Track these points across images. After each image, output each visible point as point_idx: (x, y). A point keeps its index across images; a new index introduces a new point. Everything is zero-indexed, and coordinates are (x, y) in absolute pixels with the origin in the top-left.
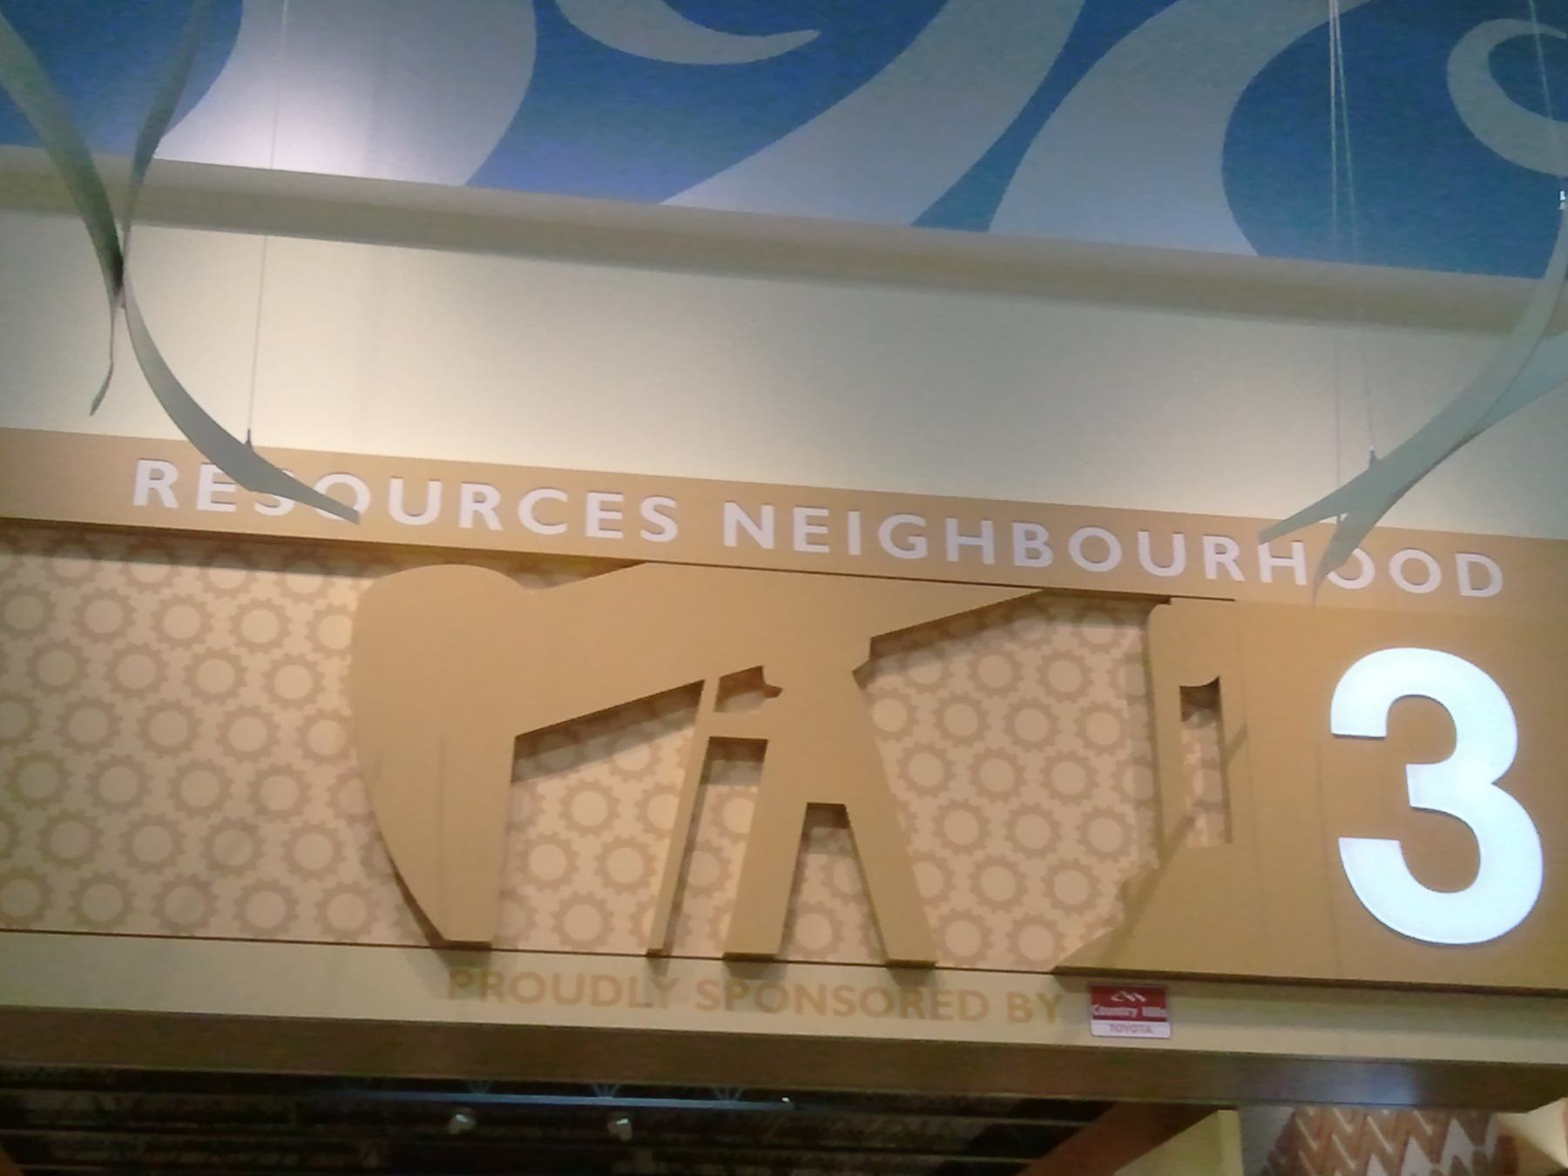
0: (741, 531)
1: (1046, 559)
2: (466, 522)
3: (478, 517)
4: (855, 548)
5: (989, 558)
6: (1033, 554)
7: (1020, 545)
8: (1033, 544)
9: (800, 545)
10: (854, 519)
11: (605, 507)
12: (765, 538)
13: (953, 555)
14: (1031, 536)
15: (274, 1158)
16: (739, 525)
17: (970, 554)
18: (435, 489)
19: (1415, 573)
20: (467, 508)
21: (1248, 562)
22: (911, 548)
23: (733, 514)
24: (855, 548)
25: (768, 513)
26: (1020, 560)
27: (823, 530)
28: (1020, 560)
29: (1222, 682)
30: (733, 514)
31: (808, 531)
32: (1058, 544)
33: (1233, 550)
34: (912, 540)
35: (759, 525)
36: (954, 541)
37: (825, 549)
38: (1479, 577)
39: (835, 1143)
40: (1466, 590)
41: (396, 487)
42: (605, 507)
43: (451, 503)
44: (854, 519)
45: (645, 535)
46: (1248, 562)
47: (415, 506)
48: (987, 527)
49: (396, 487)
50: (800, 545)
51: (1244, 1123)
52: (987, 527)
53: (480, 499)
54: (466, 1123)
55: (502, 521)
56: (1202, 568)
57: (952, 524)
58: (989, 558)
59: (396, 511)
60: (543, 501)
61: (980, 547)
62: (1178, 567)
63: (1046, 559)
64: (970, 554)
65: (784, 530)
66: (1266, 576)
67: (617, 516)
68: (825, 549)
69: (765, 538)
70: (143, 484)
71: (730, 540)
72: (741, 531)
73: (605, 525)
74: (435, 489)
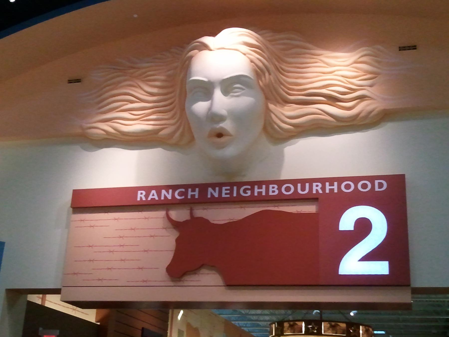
2: (314, 192)
3: (317, 190)
4: (235, 195)
5: (264, 194)
6: (273, 192)
7: (271, 189)
8: (273, 190)
9: (224, 195)
10: (235, 188)
11: (226, 190)
12: (216, 195)
16: (165, 195)
18: (307, 185)
21: (323, 188)
22: (247, 193)
23: (210, 190)
24: (235, 195)
28: (271, 194)
29: (360, 257)
30: (210, 190)
31: (262, 190)
32: (279, 189)
33: (320, 185)
34: (247, 191)
35: (165, 195)
36: (328, 187)
37: (228, 196)
38: (381, 185)
40: (377, 189)
41: (299, 185)
42: (226, 190)
44: (235, 188)
46: (323, 188)
47: (303, 189)
48: (264, 187)
49: (299, 185)
50: (224, 195)
54: (269, 103)
55: (322, 191)
56: (312, 191)
58: (264, 194)
59: (300, 191)
60: (181, 191)
61: (334, 189)
62: (307, 191)
65: (220, 192)
66: (327, 191)
67: (228, 192)
68: (228, 196)
69: (169, 197)
70: (139, 196)
73: (226, 194)
74: (307, 185)
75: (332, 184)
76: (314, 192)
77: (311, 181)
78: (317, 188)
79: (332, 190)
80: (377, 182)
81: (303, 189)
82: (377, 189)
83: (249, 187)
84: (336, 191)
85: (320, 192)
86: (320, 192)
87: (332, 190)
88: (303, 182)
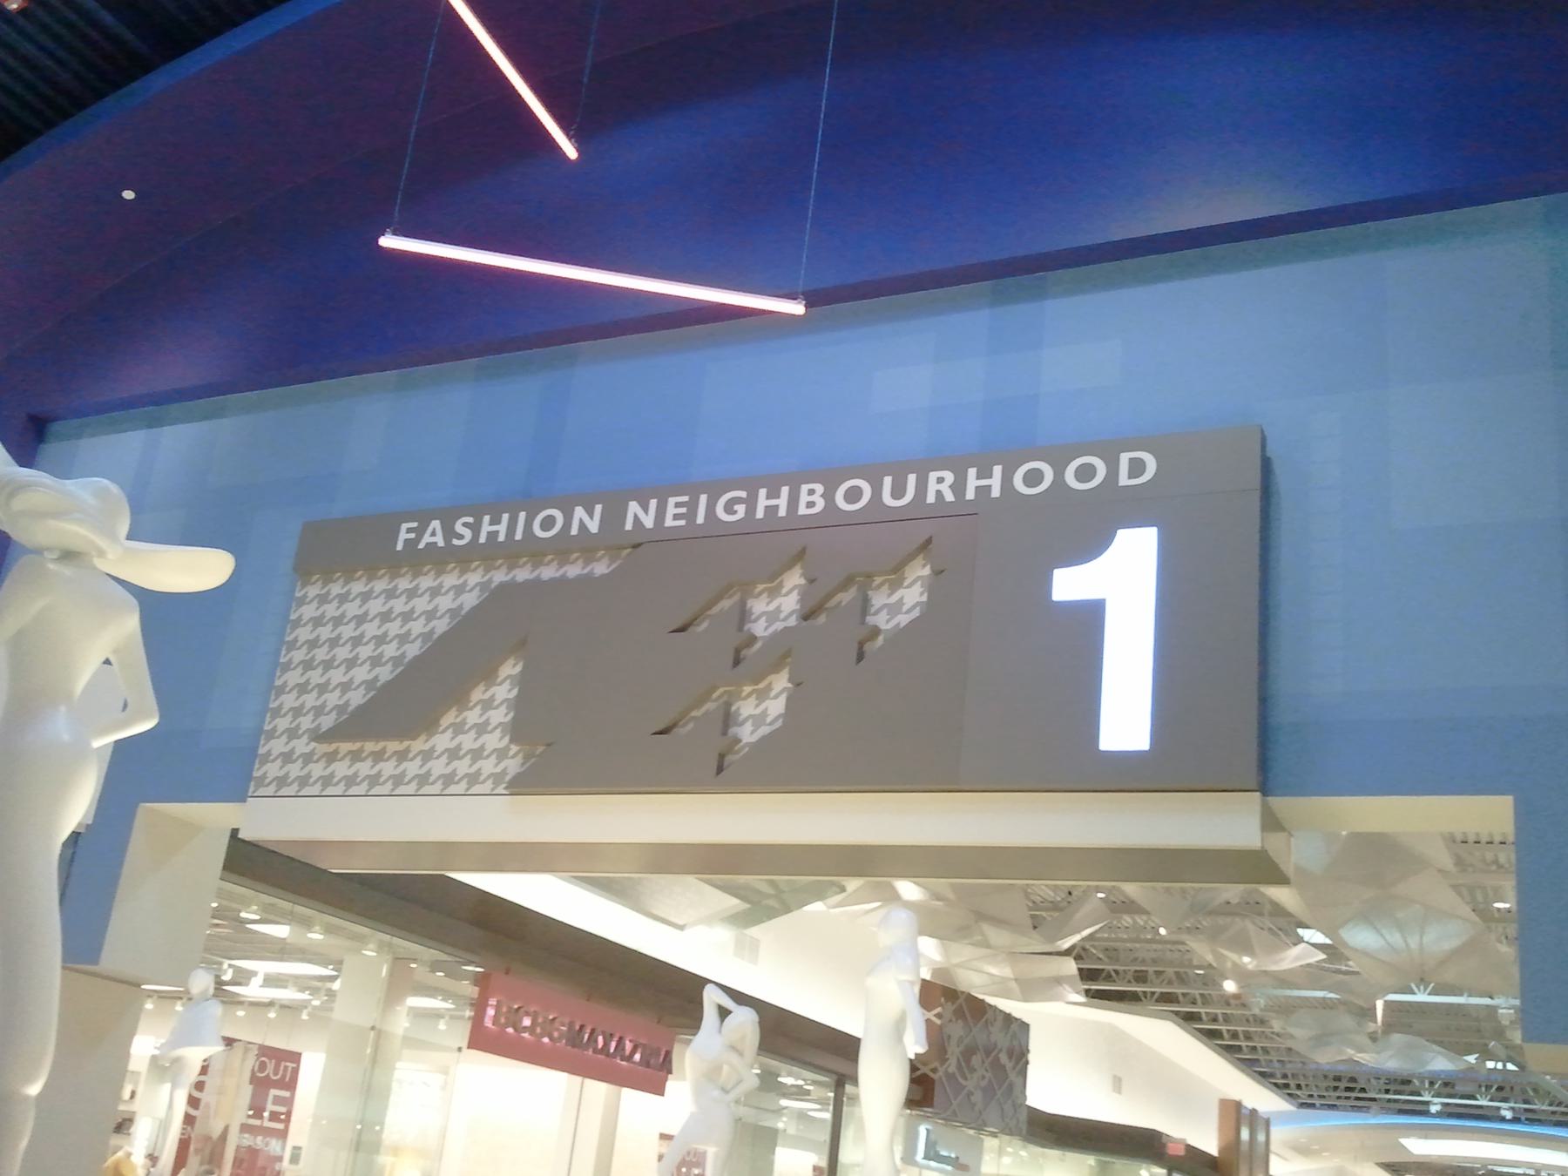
3: (939, 493)
8: (811, 498)
9: (669, 522)
11: (678, 505)
22: (736, 512)
37: (682, 523)
40: (1124, 480)
42: (678, 505)
68: (682, 523)
73: (676, 517)
79: (983, 491)
81: (898, 492)
82: (1124, 480)
83: (743, 494)
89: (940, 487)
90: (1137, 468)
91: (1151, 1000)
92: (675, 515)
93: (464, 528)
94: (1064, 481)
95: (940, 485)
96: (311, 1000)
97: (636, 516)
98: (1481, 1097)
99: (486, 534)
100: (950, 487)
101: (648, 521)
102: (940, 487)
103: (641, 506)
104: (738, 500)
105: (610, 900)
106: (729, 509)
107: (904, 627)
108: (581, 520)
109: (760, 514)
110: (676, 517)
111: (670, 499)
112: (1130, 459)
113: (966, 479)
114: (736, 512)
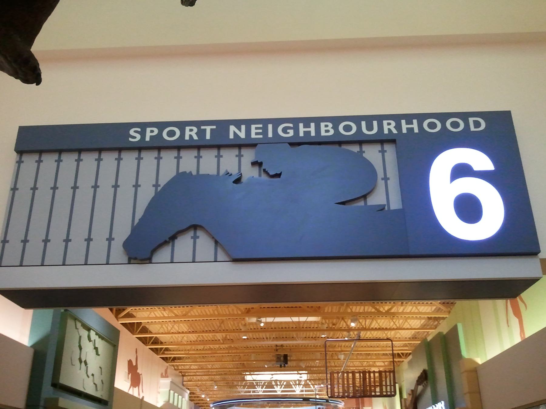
0: (235, 133)
1: (332, 132)
4: (270, 135)
5: (313, 134)
8: (327, 129)
9: (253, 136)
11: (256, 128)
12: (242, 135)
13: (301, 134)
14: (326, 126)
15: (314, 369)
17: (307, 133)
18: (375, 123)
19: (348, 128)
20: (187, 134)
21: (398, 127)
22: (289, 133)
23: (232, 128)
24: (270, 135)
25: (243, 127)
26: (323, 133)
27: (261, 131)
28: (323, 133)
30: (232, 128)
32: (335, 128)
33: (393, 124)
34: (288, 131)
35: (234, 132)
36: (302, 130)
37: (261, 136)
38: (477, 124)
39: (204, 387)
41: (363, 124)
42: (256, 128)
43: (381, 127)
44: (270, 126)
45: (131, 139)
46: (398, 127)
49: (363, 124)
50: (253, 136)
51: (376, 378)
52: (415, 121)
53: (191, 130)
57: (301, 125)
58: (313, 134)
63: (332, 132)
64: (307, 133)
66: (404, 131)
68: (261, 136)
71: (231, 136)
72: (235, 133)
73: (257, 134)
74: (375, 123)
75: (409, 122)
76: (386, 132)
77: (381, 118)
78: (389, 127)
79: (410, 130)
80: (471, 120)
82: (472, 128)
83: (291, 125)
84: (416, 130)
85: (395, 131)
86: (395, 131)
87: (410, 130)
88: (369, 119)
89: (191, 133)
90: (477, 124)
91: (269, 340)
92: (256, 133)
93: (135, 133)
94: (464, 127)
95: (191, 132)
96: (391, 309)
97: (234, 132)
98: (258, 387)
99: (195, 135)
100: (196, 133)
101: (242, 135)
102: (191, 133)
103: (238, 129)
104: (290, 128)
105: (121, 286)
106: (285, 130)
107: (159, 191)
108: (241, 132)
109: (148, 139)
110: (257, 134)
111: (186, 127)
112: (211, 129)
113: (401, 126)
114: (289, 133)
